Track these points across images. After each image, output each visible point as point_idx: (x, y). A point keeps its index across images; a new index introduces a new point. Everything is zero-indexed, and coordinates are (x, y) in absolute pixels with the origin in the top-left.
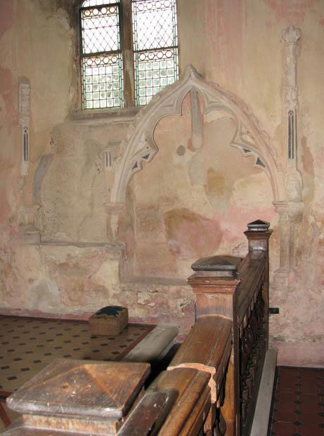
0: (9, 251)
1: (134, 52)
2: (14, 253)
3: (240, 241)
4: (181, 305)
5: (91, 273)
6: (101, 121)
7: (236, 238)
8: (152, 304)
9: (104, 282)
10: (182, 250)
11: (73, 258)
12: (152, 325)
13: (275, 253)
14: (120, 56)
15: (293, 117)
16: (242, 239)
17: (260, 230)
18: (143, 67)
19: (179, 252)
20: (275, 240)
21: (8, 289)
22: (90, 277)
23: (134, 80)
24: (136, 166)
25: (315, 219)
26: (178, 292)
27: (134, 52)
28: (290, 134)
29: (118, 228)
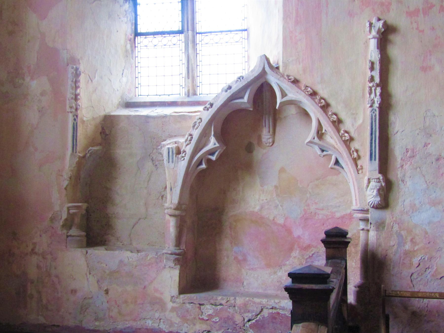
0: (49, 257)
1: (197, 33)
2: (55, 259)
3: (314, 250)
4: (249, 321)
5: (146, 283)
6: (374, 133)
7: (309, 247)
8: (217, 319)
9: (162, 294)
10: (249, 258)
11: (125, 265)
12: (323, 243)
13: (354, 264)
14: (182, 36)
15: (375, 116)
16: (316, 247)
17: (334, 240)
18: (206, 48)
19: (245, 260)
20: (353, 250)
21: (44, 301)
22: (145, 287)
23: (135, 47)
24: (323, 151)
25: (400, 228)
26: (245, 305)
27: (197, 33)
28: (372, 134)
29: (127, 250)
